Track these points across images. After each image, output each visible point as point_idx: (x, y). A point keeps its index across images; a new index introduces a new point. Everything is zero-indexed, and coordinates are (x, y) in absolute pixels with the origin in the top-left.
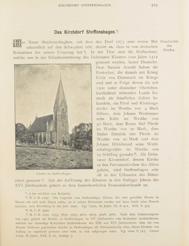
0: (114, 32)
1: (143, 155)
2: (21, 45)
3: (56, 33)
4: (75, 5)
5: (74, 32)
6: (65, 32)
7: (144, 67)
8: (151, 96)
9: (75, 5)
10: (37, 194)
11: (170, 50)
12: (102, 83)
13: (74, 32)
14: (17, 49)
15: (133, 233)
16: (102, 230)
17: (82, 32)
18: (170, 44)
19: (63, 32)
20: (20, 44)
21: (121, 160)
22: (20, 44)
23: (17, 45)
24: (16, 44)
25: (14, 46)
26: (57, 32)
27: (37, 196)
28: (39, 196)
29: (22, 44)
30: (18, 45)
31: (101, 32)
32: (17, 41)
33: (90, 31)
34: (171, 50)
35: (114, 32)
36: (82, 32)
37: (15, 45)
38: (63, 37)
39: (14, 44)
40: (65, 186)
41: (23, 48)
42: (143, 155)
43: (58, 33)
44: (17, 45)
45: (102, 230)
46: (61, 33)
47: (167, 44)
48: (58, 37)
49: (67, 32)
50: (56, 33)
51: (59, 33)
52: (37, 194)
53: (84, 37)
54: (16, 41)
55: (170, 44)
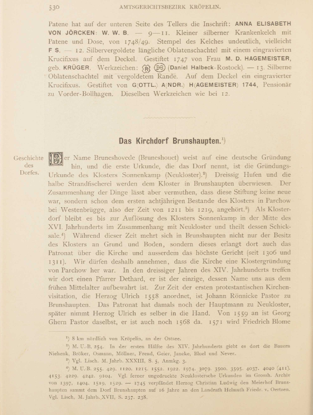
0: (217, 141)
1: (260, 210)
2: (61, 162)
3: (121, 142)
4: (126, 7)
5: (151, 141)
6: (138, 141)
7: (99, 201)
8: (279, 248)
9: (126, 7)
10: (85, 339)
11: (30, 173)
12: (224, 227)
13: (151, 141)
14: (56, 169)
15: (285, 392)
16: (256, 386)
17: (165, 142)
18: (30, 162)
19: (134, 141)
20: (60, 160)
21: (126, 184)
22: (60, 160)
23: (56, 162)
24: (54, 160)
25: (50, 164)
26: (124, 141)
27: (85, 342)
28: (90, 342)
29: (64, 161)
30: (58, 162)
31: (189, 142)
32: (56, 154)
33: (210, 140)
34: (32, 173)
35: (217, 141)
36: (165, 142)
37: (53, 163)
38: (134, 149)
39: (50, 160)
40: (269, 347)
41: (66, 168)
42: (260, 210)
43: (126, 142)
44: (56, 162)
45: (256, 386)
46: (130, 142)
47: (24, 162)
48: (125, 149)
49: (140, 141)
50: (121, 142)
51: (128, 142)
52: (85, 339)
53: (169, 149)
54: (54, 156)
55: (30, 162)
